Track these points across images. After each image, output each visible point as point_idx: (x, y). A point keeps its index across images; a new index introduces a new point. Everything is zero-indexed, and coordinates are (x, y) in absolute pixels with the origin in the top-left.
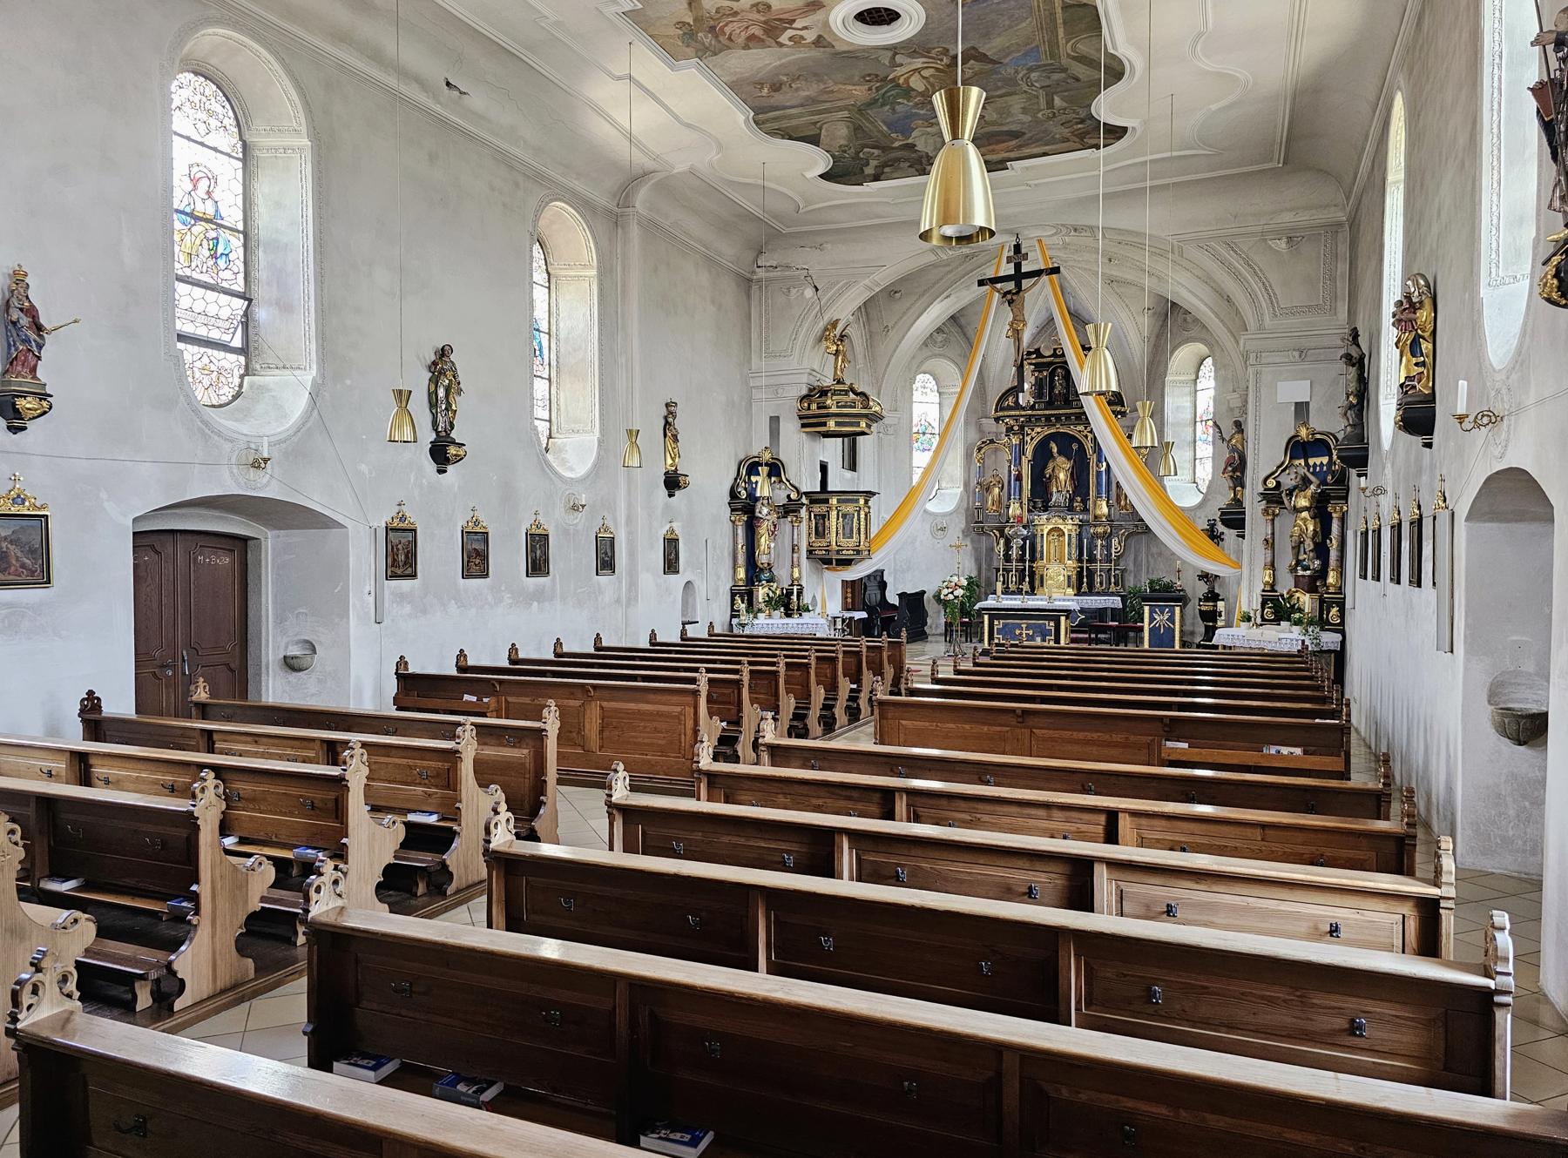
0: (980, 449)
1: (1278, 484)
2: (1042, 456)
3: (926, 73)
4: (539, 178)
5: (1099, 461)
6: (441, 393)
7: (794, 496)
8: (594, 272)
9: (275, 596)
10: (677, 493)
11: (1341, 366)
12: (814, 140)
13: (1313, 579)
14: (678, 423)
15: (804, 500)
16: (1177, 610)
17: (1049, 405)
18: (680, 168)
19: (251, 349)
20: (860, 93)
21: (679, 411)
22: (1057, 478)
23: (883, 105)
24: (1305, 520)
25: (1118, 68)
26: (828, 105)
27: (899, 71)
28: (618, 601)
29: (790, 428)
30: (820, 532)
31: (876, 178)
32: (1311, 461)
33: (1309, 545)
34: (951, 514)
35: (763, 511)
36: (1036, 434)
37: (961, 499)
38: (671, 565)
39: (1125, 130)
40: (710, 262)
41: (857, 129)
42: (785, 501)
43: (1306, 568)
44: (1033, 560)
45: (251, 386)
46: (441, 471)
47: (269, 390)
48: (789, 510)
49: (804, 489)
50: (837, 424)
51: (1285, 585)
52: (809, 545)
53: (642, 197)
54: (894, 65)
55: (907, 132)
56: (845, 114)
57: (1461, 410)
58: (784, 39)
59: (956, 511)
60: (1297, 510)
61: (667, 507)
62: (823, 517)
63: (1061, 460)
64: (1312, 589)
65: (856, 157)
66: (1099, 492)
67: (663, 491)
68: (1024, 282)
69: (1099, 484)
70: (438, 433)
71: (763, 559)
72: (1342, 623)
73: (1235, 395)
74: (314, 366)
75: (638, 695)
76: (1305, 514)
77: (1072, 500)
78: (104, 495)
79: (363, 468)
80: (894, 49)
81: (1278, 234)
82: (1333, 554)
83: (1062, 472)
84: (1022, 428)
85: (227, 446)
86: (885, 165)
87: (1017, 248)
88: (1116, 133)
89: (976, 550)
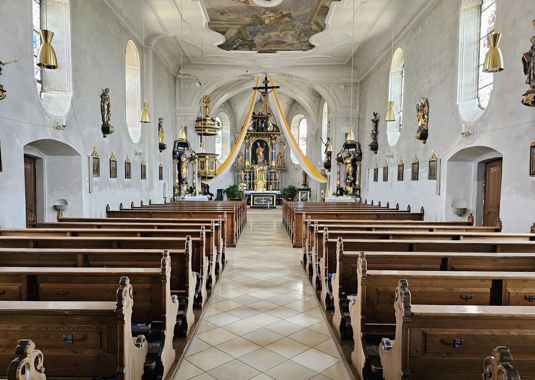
2: (255, 146)
3: (271, 18)
4: (126, 31)
5: (272, 149)
6: (106, 107)
7: (193, 154)
8: (126, 66)
9: (48, 182)
10: (163, 151)
11: (372, 123)
12: (223, 33)
13: (351, 183)
14: (163, 125)
15: (197, 156)
16: (308, 193)
17: (257, 131)
18: (172, 35)
19: (43, 82)
20: (248, 20)
21: (163, 121)
25: (324, 27)
26: (235, 23)
27: (265, 16)
28: (146, 189)
29: (192, 131)
30: (202, 168)
31: (235, 49)
32: (350, 150)
33: (351, 174)
35: (183, 159)
36: (254, 139)
38: (161, 177)
39: (314, 46)
40: (167, 70)
41: (239, 32)
42: (190, 156)
44: (253, 179)
45: (45, 97)
46: (104, 137)
47: (53, 99)
48: (192, 159)
50: (209, 131)
53: (154, 42)
54: (264, 14)
55: (254, 36)
56: (239, 26)
57: (463, 132)
60: (347, 164)
61: (160, 156)
62: (204, 162)
63: (260, 148)
64: (351, 186)
65: (233, 42)
66: (272, 159)
67: (159, 150)
69: (272, 156)
70: (104, 121)
71: (184, 176)
74: (72, 91)
75: (210, 215)
77: (264, 161)
78: (15, 135)
79: (85, 133)
80: (267, 9)
81: (342, 84)
82: (358, 176)
83: (260, 151)
84: (249, 137)
85: (49, 119)
87: (266, 79)
88: (312, 47)
89: (234, 176)
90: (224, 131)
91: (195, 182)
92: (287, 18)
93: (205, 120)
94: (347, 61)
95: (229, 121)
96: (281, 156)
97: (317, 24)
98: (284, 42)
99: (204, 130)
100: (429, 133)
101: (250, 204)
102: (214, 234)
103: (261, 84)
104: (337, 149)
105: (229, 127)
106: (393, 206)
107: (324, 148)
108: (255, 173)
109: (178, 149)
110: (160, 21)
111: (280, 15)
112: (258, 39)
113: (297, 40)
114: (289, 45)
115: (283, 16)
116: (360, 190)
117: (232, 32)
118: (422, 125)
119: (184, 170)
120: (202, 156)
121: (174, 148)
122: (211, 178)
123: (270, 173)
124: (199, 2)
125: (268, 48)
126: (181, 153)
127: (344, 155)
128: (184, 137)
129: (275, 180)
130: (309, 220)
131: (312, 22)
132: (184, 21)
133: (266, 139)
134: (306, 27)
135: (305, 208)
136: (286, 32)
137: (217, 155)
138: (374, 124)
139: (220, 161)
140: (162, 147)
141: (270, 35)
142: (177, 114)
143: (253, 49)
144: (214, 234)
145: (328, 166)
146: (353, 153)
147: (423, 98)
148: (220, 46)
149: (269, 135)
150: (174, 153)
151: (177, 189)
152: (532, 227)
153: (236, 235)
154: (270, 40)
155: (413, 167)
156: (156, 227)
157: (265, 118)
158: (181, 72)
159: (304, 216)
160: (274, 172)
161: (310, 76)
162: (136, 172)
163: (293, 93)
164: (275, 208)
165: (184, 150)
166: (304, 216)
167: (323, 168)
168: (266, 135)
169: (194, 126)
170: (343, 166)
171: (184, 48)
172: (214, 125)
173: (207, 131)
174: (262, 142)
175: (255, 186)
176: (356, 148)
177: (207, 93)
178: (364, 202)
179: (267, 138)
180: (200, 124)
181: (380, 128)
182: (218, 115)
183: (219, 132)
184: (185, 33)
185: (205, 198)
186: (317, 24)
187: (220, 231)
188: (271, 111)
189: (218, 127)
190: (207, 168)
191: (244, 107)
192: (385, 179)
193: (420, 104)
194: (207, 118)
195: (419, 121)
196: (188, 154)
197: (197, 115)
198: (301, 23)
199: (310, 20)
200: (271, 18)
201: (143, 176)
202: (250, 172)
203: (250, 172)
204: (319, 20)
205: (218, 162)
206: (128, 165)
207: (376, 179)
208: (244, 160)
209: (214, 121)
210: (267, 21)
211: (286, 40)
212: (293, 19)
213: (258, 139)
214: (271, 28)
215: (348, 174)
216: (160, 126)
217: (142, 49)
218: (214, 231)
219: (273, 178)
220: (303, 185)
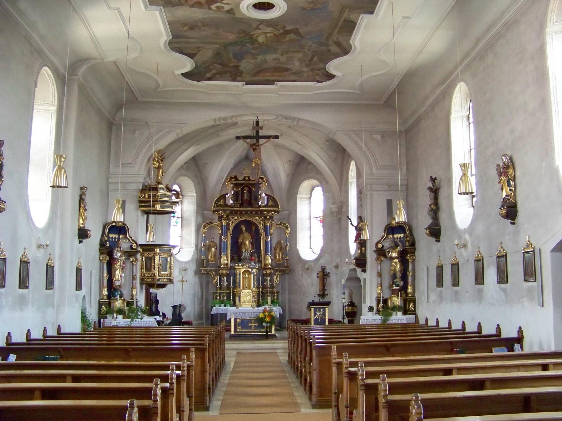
0: (205, 227)
1: (383, 246)
2: (237, 230)
3: (268, 35)
4: (40, 53)
5: (267, 235)
7: (134, 246)
10: (84, 241)
11: (428, 193)
13: (400, 290)
14: (87, 198)
15: (139, 249)
17: (241, 205)
18: (111, 59)
20: (232, 37)
21: (88, 192)
22: (245, 244)
23: (239, 45)
24: (396, 263)
27: (258, 31)
29: (132, 206)
30: (149, 267)
31: (209, 79)
32: (396, 236)
33: (399, 275)
34: (188, 262)
36: (237, 219)
37: (194, 254)
38: (79, 286)
41: (218, 54)
43: (397, 286)
44: (235, 287)
48: (131, 254)
49: (140, 242)
50: (161, 206)
51: (387, 294)
52: (141, 275)
54: (257, 28)
56: (217, 46)
58: (213, 7)
59: (191, 261)
60: (392, 258)
63: (247, 235)
67: (77, 240)
68: (260, 140)
72: (415, 311)
73: (334, 206)
76: (396, 260)
80: (262, 22)
84: (227, 216)
86: (219, 73)
87: (257, 123)
88: (330, 77)
90: (187, 208)
91: (135, 293)
92: (292, 36)
93: (156, 189)
94: (384, 98)
95: (194, 190)
96: (280, 246)
97: (338, 44)
98: (287, 70)
99: (154, 206)
100: (520, 208)
101: (230, 330)
102: (175, 391)
103: (247, 131)
104: (374, 234)
105: (194, 200)
106: (457, 326)
107: (352, 233)
108: (238, 277)
109: (109, 237)
110: (94, 40)
111: (281, 31)
112: (246, 65)
113: (307, 66)
114: (295, 73)
115: (287, 32)
116: (414, 302)
117: (207, 54)
118: (507, 195)
119: (117, 272)
120: (148, 248)
121: (103, 235)
122: (163, 286)
123: (264, 275)
124: (157, 12)
125: (262, 76)
126: (115, 244)
127: (387, 244)
128: (121, 218)
129: (272, 287)
130: (346, 360)
131: (330, 42)
132: (133, 38)
133: (256, 219)
134: (323, 48)
135: (329, 338)
136: (291, 54)
137: (174, 247)
138: (433, 194)
139: (177, 256)
140: (83, 234)
141: (265, 59)
142: (110, 180)
143: (238, 78)
144: (175, 391)
145: (361, 262)
146: (402, 244)
147: (505, 155)
148: (185, 75)
149: (260, 213)
150: (102, 244)
151: (106, 307)
152: (430, 205)
153: (209, 388)
154: (266, 66)
155: (498, 263)
156: (69, 378)
157: (253, 185)
158: (123, 113)
159: (334, 353)
160: (270, 275)
161: (327, 120)
162: (37, 276)
163: (300, 147)
164: (273, 336)
165: (119, 239)
166: (334, 353)
167: (353, 267)
168: (256, 212)
169: (137, 200)
170: (386, 263)
171: (128, 78)
172: (170, 197)
173: (158, 207)
174: (249, 224)
175: (237, 299)
176: (404, 232)
177: (161, 145)
178: (422, 322)
179: (257, 218)
180: (147, 196)
181: (442, 201)
182: (178, 181)
183: (177, 209)
184: (132, 56)
185: (150, 321)
186: (338, 44)
187: (184, 385)
188: (264, 173)
189: (177, 200)
190: (157, 270)
191: (220, 168)
192: (456, 282)
193: (501, 165)
194: (160, 186)
195: (502, 189)
196: (125, 245)
197: (142, 180)
198: (314, 43)
199: (328, 39)
200: (268, 35)
201: (50, 284)
202: (228, 276)
203: (228, 276)
204: (341, 39)
205: (175, 258)
206: (25, 265)
207: (440, 282)
208: (218, 254)
209: (170, 190)
210: (261, 39)
211: (290, 67)
212: (303, 37)
213: (243, 219)
214: (267, 48)
215: (394, 276)
216: (81, 200)
217: (63, 81)
218: (175, 385)
219: (268, 284)
220: (319, 295)
